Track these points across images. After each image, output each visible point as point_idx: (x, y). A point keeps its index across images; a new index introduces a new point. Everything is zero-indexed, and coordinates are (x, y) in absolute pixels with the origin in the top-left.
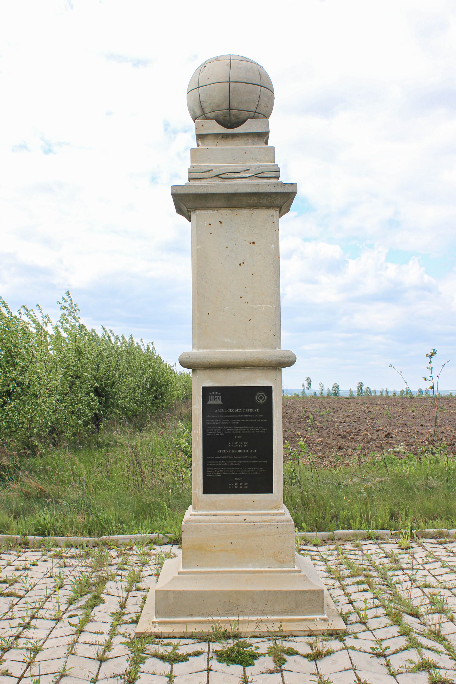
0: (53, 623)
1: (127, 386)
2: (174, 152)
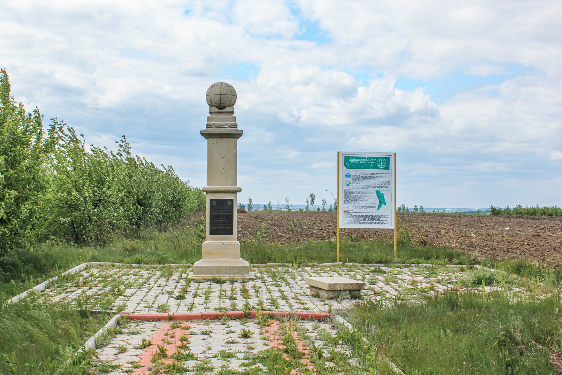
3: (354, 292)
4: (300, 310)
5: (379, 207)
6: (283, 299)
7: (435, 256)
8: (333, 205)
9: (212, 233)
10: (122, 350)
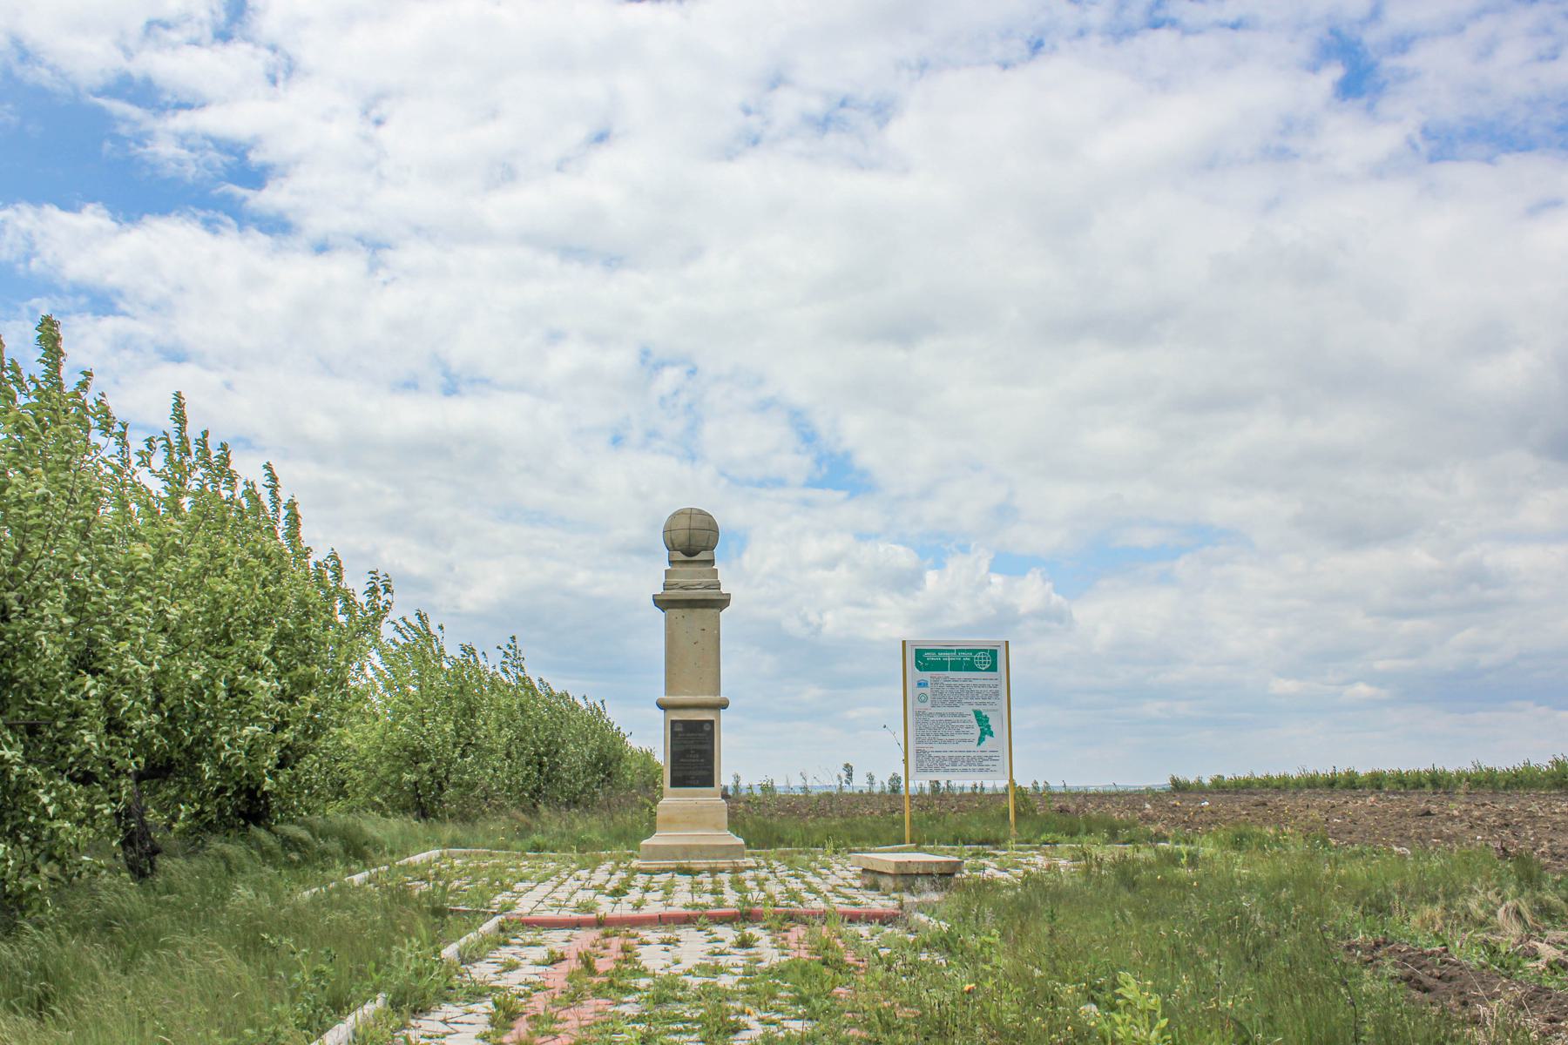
1: (575, 754)
2: (652, 575)
3: (944, 876)
7: (1083, 827)
10: (511, 967)
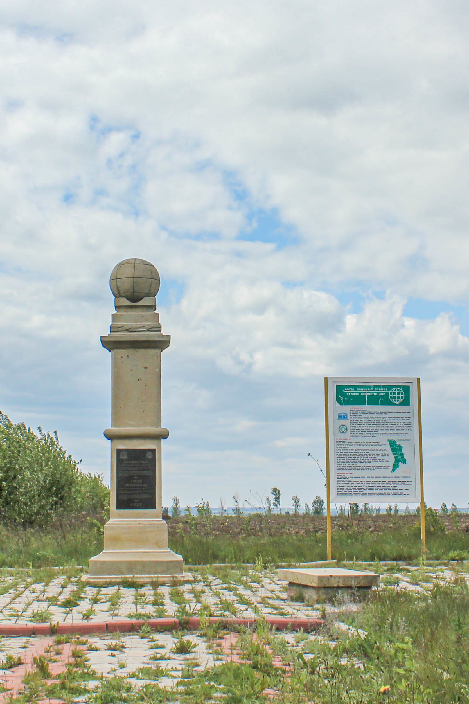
0: (228, 218)
1: (31, 480)
3: (362, 589)
4: (273, 616)
5: (395, 467)
6: (242, 603)
8: (310, 507)
9: (120, 505)
